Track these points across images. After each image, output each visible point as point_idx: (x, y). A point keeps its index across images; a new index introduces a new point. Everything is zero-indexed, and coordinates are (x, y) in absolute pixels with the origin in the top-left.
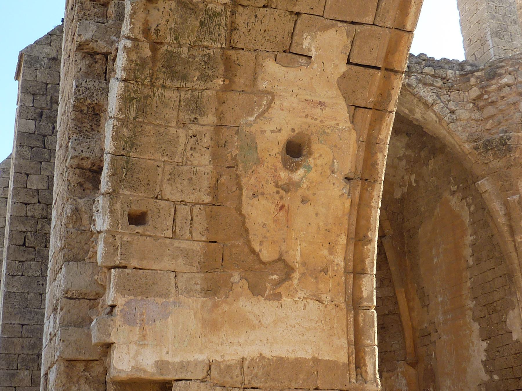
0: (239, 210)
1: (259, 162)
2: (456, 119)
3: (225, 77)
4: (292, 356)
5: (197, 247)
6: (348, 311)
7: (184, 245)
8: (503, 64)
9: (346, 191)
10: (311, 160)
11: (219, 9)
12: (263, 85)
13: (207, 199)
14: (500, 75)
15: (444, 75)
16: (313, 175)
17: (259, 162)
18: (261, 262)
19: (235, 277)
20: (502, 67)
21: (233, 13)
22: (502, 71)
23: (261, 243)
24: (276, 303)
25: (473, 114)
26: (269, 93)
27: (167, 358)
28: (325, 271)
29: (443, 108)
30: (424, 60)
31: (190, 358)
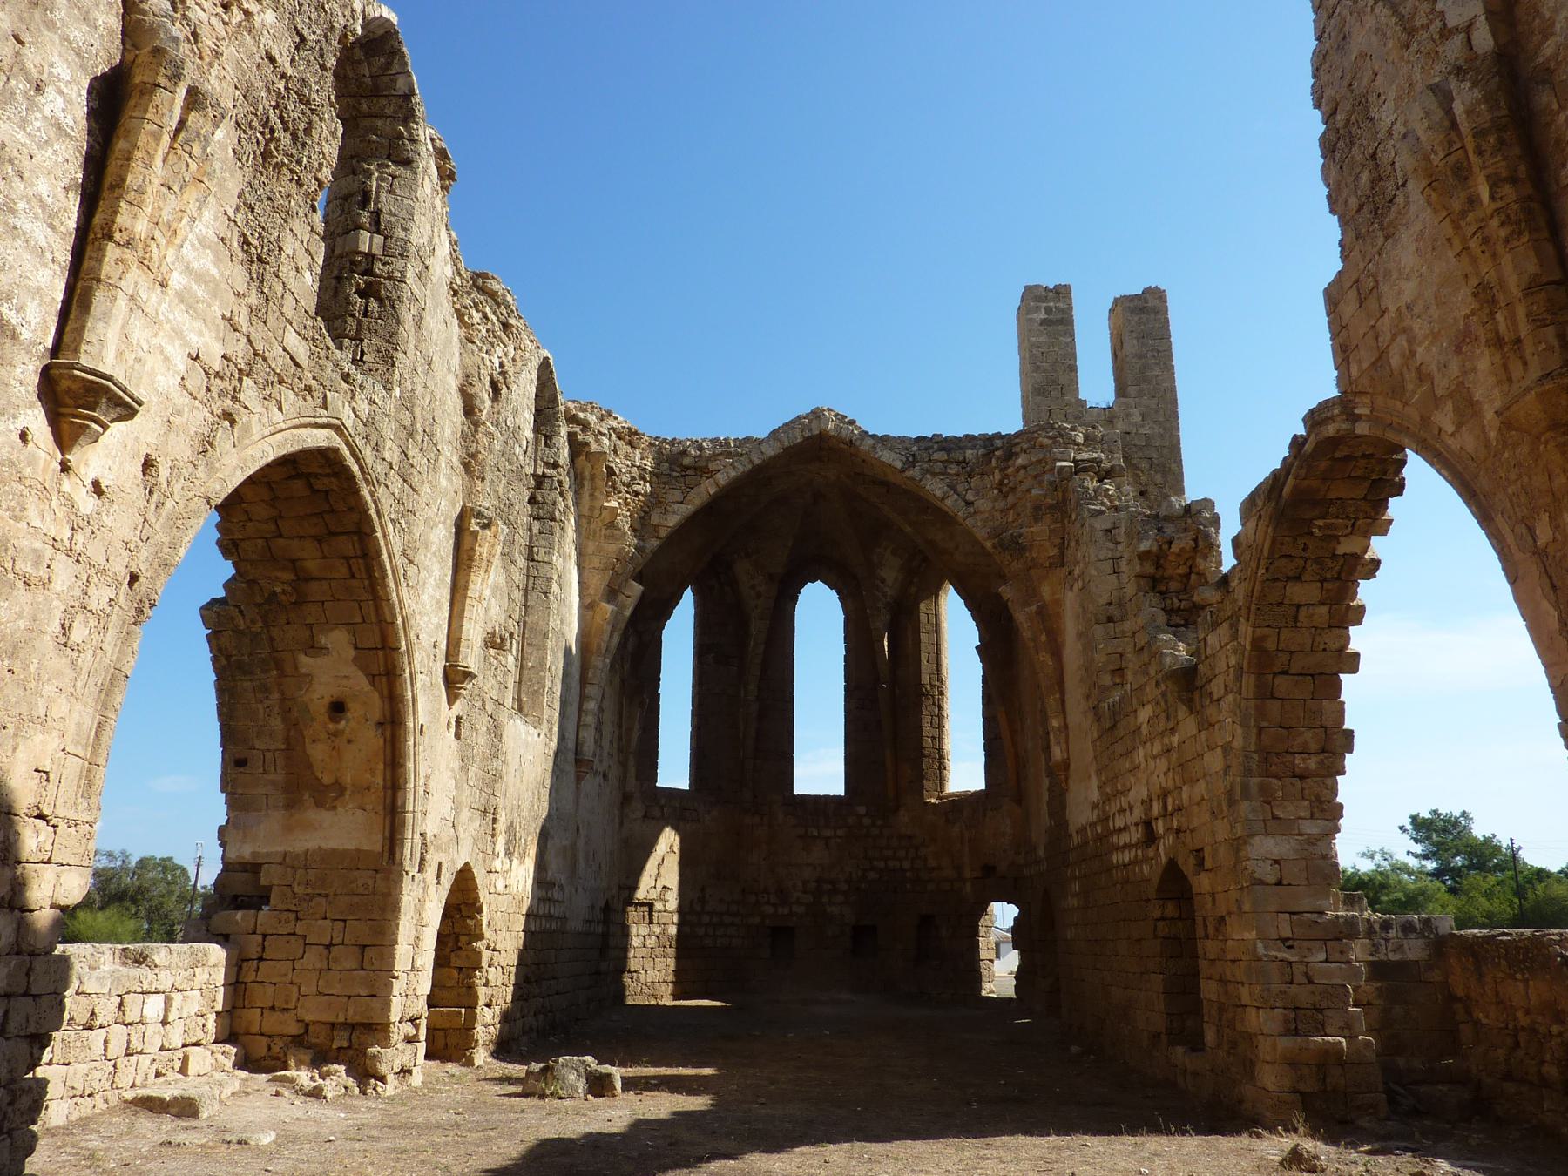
0: (304, 751)
1: (313, 720)
2: (975, 512)
3: (277, 669)
4: (341, 847)
5: (280, 778)
6: (385, 818)
7: (271, 777)
8: (1018, 440)
9: (379, 732)
10: (349, 714)
11: (259, 630)
12: (303, 671)
13: (283, 747)
14: (1017, 455)
15: (961, 459)
16: (352, 724)
17: (313, 720)
18: (324, 785)
19: (306, 796)
20: (1018, 444)
21: (268, 631)
22: (1017, 449)
23: (322, 772)
24: (332, 812)
25: (997, 504)
26: (309, 675)
27: (257, 850)
28: (368, 789)
29: (956, 500)
30: (937, 443)
31: (273, 849)
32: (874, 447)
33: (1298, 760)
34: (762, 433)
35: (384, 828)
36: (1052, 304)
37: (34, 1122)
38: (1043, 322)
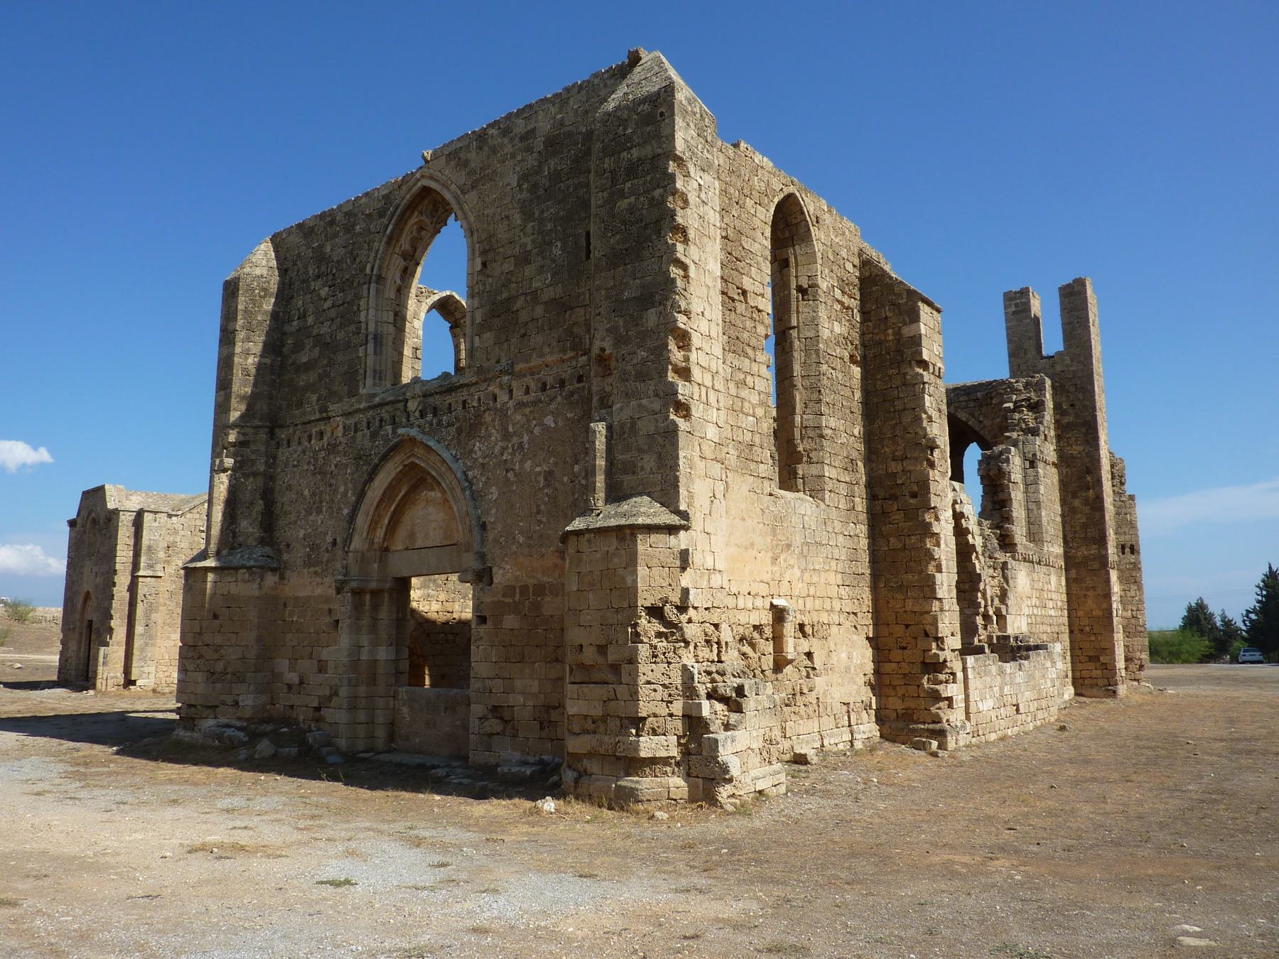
35: (224, 384)
36: (1018, 301)
38: (1014, 313)
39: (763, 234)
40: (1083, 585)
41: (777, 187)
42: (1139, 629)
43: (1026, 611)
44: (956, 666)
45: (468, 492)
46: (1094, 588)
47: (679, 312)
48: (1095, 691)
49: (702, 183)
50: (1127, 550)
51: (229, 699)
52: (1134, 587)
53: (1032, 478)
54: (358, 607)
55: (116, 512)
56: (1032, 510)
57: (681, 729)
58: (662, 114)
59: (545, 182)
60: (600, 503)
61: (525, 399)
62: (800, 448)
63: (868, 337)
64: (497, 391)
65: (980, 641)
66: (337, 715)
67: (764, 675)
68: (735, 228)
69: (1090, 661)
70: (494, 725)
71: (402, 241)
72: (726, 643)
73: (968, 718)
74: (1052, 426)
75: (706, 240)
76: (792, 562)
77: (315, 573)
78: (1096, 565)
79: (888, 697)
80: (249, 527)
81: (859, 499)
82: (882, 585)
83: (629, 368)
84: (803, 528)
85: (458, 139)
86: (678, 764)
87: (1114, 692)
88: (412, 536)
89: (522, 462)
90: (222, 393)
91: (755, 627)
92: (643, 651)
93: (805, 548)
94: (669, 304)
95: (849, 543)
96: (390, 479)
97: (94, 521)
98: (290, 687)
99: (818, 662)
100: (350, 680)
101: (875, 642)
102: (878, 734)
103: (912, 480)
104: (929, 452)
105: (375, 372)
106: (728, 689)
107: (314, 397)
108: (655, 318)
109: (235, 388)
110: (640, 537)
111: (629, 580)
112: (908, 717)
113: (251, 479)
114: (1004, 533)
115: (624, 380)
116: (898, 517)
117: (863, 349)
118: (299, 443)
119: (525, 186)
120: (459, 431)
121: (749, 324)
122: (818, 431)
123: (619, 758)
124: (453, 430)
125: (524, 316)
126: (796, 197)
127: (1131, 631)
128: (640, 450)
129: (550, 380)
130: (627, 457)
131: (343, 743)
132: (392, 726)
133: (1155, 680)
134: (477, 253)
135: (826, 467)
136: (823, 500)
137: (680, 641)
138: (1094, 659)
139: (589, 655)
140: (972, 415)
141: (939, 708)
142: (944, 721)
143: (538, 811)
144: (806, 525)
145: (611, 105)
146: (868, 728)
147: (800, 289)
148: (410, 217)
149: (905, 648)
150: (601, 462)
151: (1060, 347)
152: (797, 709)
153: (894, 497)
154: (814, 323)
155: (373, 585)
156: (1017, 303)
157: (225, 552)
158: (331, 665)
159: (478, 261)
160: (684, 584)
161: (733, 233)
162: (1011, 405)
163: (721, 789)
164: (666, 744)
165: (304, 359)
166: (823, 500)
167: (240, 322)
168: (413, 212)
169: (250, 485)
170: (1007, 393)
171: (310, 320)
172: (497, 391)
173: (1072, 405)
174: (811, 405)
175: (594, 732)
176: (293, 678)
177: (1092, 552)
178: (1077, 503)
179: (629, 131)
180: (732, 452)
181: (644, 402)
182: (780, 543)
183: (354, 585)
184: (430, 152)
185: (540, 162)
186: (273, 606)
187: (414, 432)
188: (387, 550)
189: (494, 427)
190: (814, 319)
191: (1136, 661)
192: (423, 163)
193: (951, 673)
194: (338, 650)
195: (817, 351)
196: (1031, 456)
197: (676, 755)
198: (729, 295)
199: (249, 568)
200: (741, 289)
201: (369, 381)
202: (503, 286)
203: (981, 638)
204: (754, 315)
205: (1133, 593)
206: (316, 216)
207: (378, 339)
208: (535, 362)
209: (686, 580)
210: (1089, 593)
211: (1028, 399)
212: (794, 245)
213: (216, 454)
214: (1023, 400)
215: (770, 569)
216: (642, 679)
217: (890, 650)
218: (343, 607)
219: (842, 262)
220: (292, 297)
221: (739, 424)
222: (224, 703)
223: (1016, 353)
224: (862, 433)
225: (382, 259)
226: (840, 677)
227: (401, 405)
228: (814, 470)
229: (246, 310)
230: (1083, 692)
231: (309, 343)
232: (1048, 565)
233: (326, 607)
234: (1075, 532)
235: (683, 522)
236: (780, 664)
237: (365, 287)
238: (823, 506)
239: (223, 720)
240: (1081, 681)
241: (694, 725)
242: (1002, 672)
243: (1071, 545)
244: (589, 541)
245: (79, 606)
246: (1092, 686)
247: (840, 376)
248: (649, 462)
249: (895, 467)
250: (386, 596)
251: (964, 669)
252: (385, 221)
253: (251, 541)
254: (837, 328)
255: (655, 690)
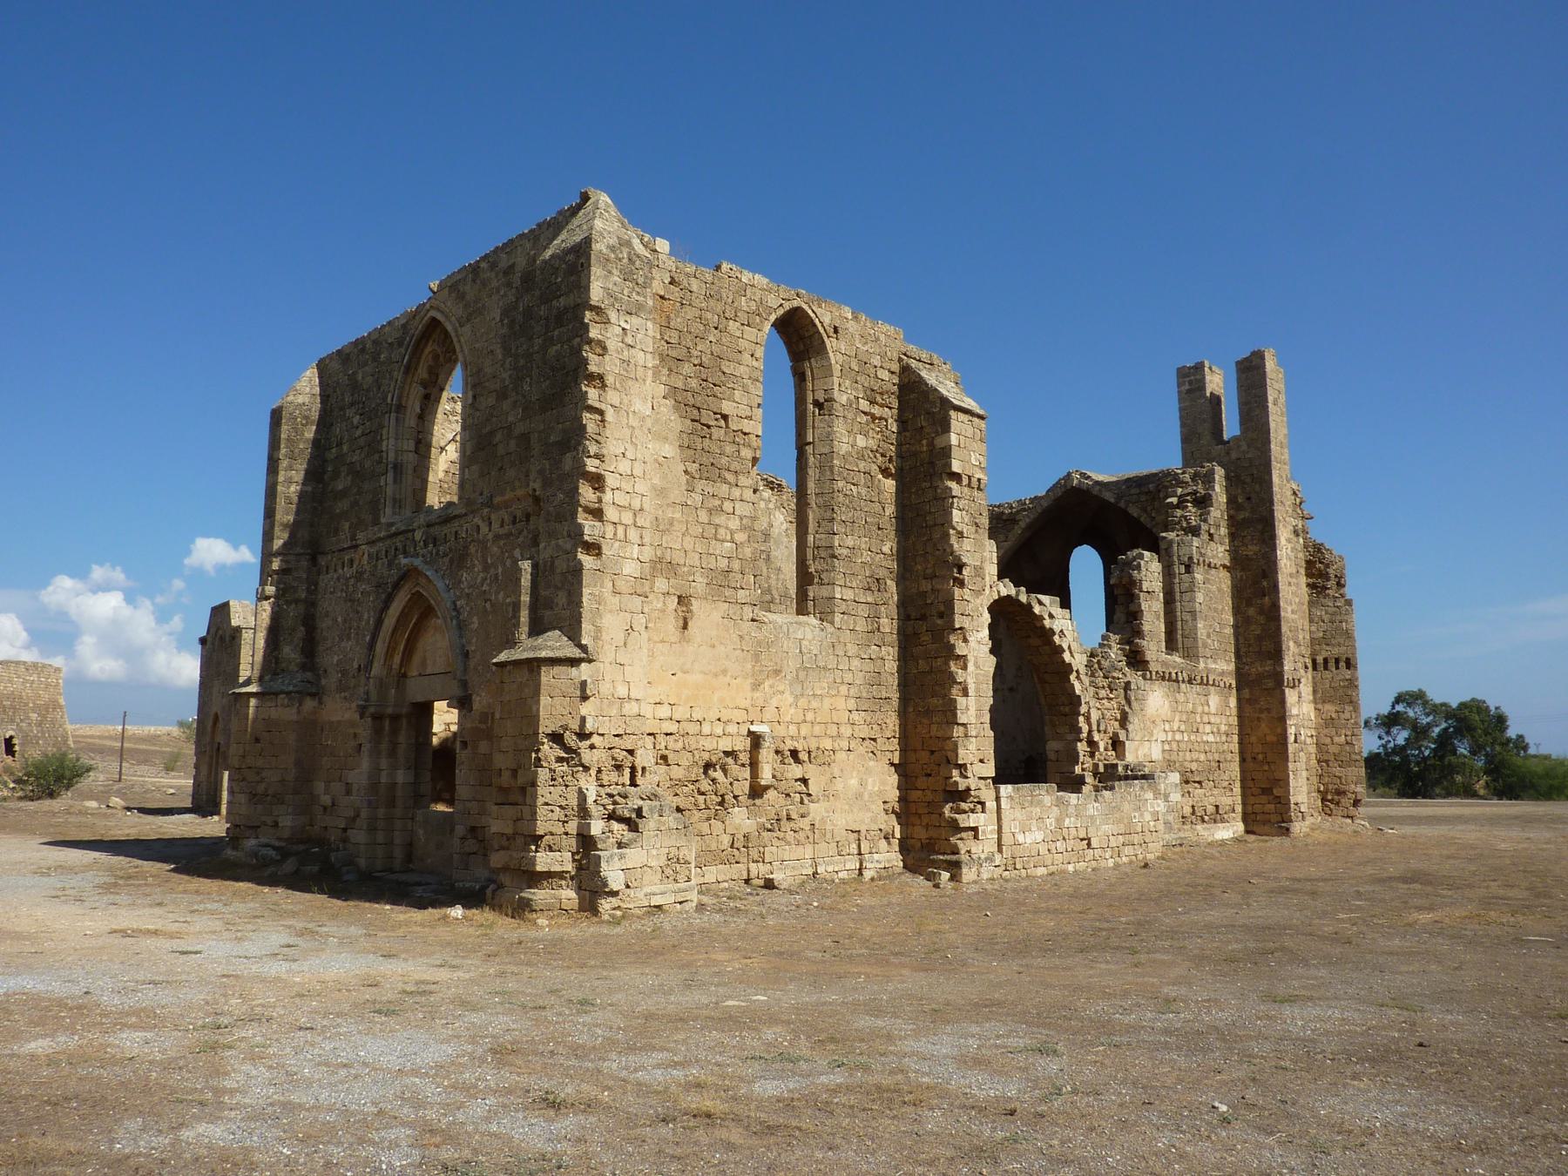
32: (1100, 490)
33: (1062, 708)
34: (1042, 493)
35: (270, 513)
37: (450, 504)
38: (1188, 391)
39: (752, 356)
40: (1258, 706)
41: (773, 301)
42: (1354, 757)
43: (1162, 737)
44: (987, 794)
45: (454, 622)
46: (1268, 710)
47: (590, 457)
48: (1267, 828)
49: (627, 327)
50: (1342, 664)
51: (269, 821)
52: (1348, 708)
53: (1187, 585)
54: (378, 732)
55: (238, 630)
56: (1187, 621)
57: (575, 846)
58: (582, 265)
59: (520, 318)
60: (524, 636)
61: (502, 531)
62: (812, 570)
63: (904, 448)
64: (480, 523)
65: (1083, 770)
66: (359, 836)
67: (737, 801)
68: (712, 354)
69: (1263, 793)
70: (471, 845)
71: (420, 371)
72: (644, 769)
73: (1000, 850)
74: (1224, 523)
75: (630, 383)
76: (781, 688)
77: (345, 698)
78: (1270, 684)
79: (913, 825)
80: (290, 652)
81: (886, 620)
82: (911, 710)
83: (551, 509)
84: (801, 652)
85: (459, 271)
86: (572, 878)
87: (1288, 829)
88: (424, 663)
89: (497, 593)
90: (268, 521)
91: (727, 754)
92: (543, 775)
93: (802, 675)
94: (581, 449)
95: (869, 666)
96: (401, 607)
97: (222, 639)
98: (325, 808)
99: (813, 789)
100: (370, 802)
101: (901, 768)
102: (901, 864)
103: (940, 599)
104: (955, 570)
105: (394, 500)
106: (625, 811)
107: (347, 525)
108: (571, 463)
109: (278, 517)
110: (543, 669)
111: (534, 708)
112: (930, 847)
113: (293, 606)
114: (1133, 649)
115: (548, 521)
116: (926, 638)
117: (899, 461)
118: (335, 570)
119: (506, 321)
120: (451, 561)
121: (729, 449)
122: (830, 551)
123: (524, 872)
124: (446, 560)
125: (501, 450)
126: (803, 310)
127: (1344, 759)
128: (557, 588)
129: (519, 514)
130: (547, 593)
131: (362, 862)
132: (410, 846)
133: (1372, 819)
134: (469, 387)
135: (838, 589)
136: (832, 623)
137: (577, 766)
138: (1266, 791)
139: (506, 779)
140: (1145, 510)
141: (961, 839)
142: (963, 852)
143: (446, 917)
144: (804, 650)
145: (548, 253)
146: (888, 856)
147: (817, 404)
148: (426, 345)
149: (930, 775)
150: (525, 598)
151: (1237, 432)
152: (781, 835)
153: (923, 618)
154: (829, 438)
155: (390, 710)
156: (1191, 379)
157: (267, 678)
158: (355, 787)
159: (470, 394)
160: (584, 712)
161: (710, 359)
162: (1174, 500)
163: (603, 901)
164: (561, 859)
165: (340, 487)
166: (832, 623)
167: (283, 451)
168: (428, 341)
169: (293, 612)
170: (1172, 486)
171: (345, 448)
172: (480, 523)
173: (1249, 499)
174: (824, 523)
175: (508, 849)
176: (326, 800)
177: (1267, 669)
178: (1251, 611)
179: (559, 279)
180: (699, 579)
181: (560, 542)
182: (764, 669)
183: (372, 710)
184: (438, 282)
185: (517, 298)
186: (310, 729)
187: (417, 562)
188: (405, 676)
189: (477, 559)
190: (829, 434)
191: (1350, 795)
192: (432, 294)
193: (979, 803)
194: (360, 773)
195: (831, 468)
196: (1186, 559)
197: (570, 869)
198: (702, 421)
199: (288, 693)
200: (720, 414)
201: (388, 510)
202: (487, 420)
203: (1084, 766)
204: (737, 439)
205: (1347, 715)
206: (352, 343)
207: (398, 468)
208: (509, 495)
209: (586, 709)
210: (1263, 716)
211: (1195, 492)
212: (810, 358)
213: (263, 583)
214: (1188, 494)
215: (749, 695)
216: (540, 801)
217: (916, 777)
218: (364, 731)
219: (873, 370)
220: (332, 425)
221: (711, 551)
222: (265, 824)
223: (1189, 438)
224: (895, 550)
225: (402, 388)
226: (847, 804)
227: (410, 534)
228: (824, 592)
229: (289, 440)
230: (1255, 829)
231: (344, 469)
232: (1207, 684)
233: (351, 731)
234: (1250, 645)
235: (583, 655)
236: (757, 791)
237: (387, 416)
238: (830, 629)
239: (263, 840)
240: (1253, 816)
241: (586, 842)
242: (1060, 803)
243: (1244, 660)
244: (509, 672)
245: (209, 729)
246: (1264, 823)
247: (863, 491)
248: (561, 599)
249: (926, 586)
250: (404, 721)
251: (998, 799)
252: (403, 350)
253: (293, 667)
254: (861, 442)
255: (552, 811)
